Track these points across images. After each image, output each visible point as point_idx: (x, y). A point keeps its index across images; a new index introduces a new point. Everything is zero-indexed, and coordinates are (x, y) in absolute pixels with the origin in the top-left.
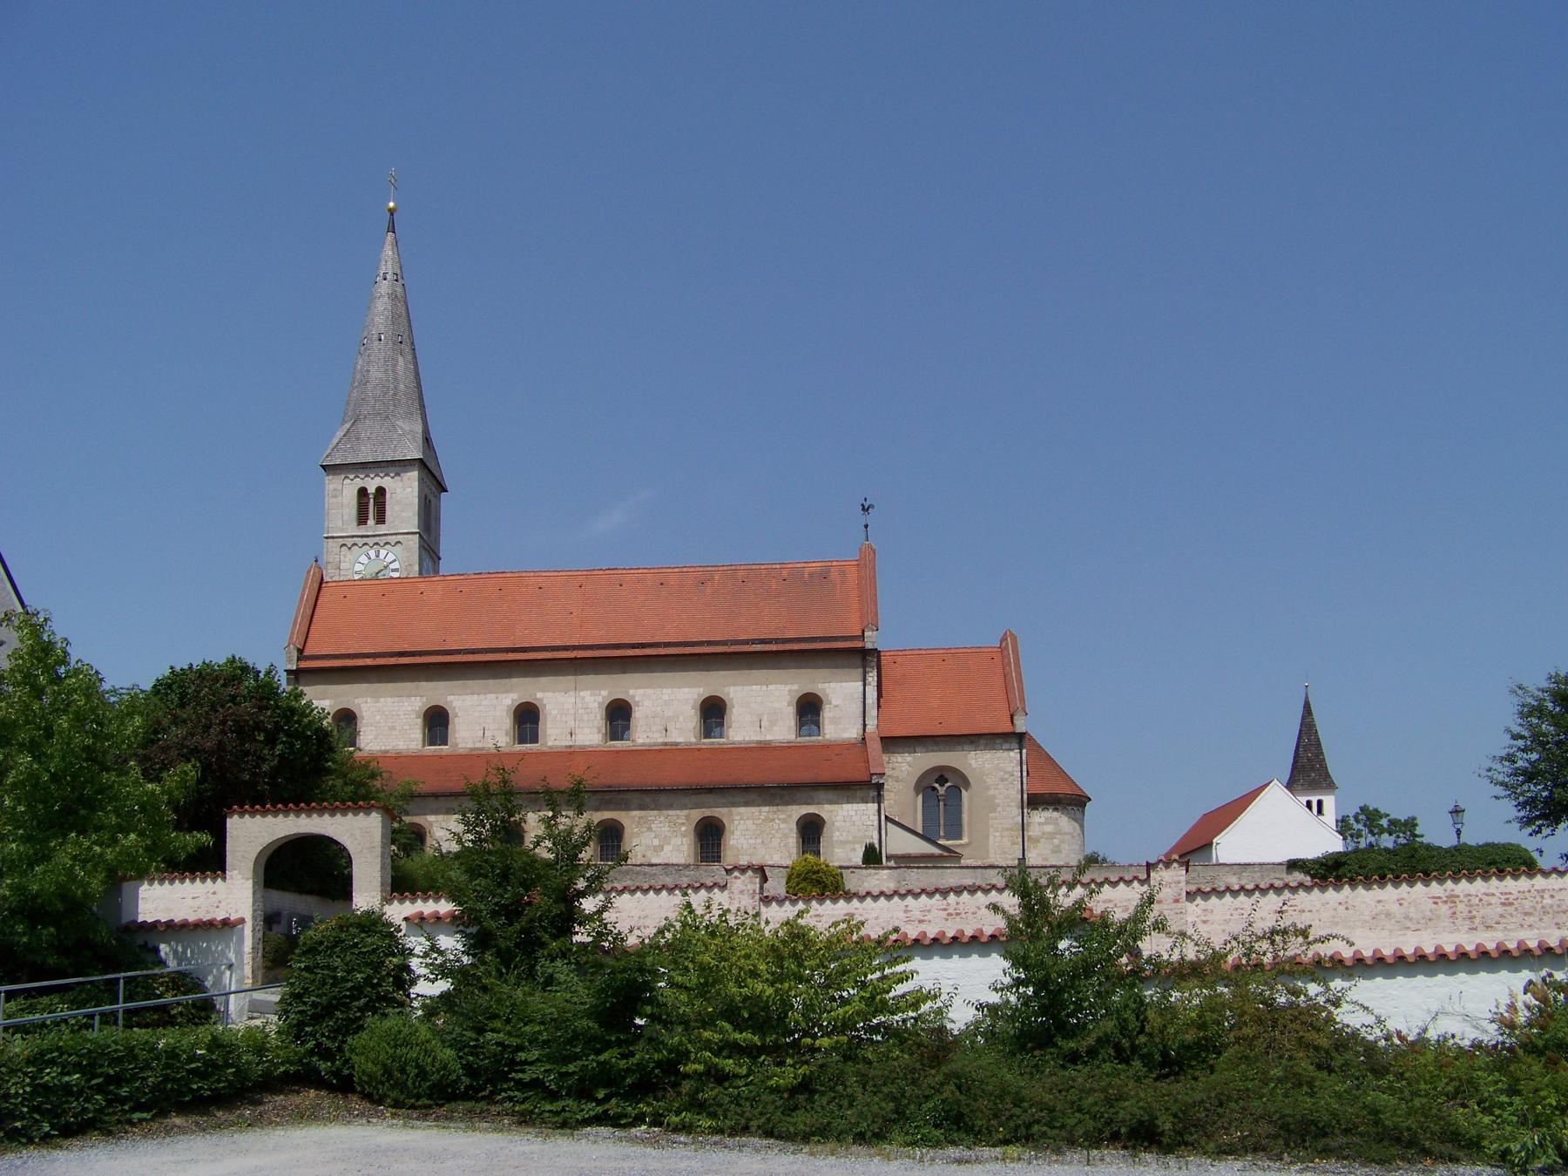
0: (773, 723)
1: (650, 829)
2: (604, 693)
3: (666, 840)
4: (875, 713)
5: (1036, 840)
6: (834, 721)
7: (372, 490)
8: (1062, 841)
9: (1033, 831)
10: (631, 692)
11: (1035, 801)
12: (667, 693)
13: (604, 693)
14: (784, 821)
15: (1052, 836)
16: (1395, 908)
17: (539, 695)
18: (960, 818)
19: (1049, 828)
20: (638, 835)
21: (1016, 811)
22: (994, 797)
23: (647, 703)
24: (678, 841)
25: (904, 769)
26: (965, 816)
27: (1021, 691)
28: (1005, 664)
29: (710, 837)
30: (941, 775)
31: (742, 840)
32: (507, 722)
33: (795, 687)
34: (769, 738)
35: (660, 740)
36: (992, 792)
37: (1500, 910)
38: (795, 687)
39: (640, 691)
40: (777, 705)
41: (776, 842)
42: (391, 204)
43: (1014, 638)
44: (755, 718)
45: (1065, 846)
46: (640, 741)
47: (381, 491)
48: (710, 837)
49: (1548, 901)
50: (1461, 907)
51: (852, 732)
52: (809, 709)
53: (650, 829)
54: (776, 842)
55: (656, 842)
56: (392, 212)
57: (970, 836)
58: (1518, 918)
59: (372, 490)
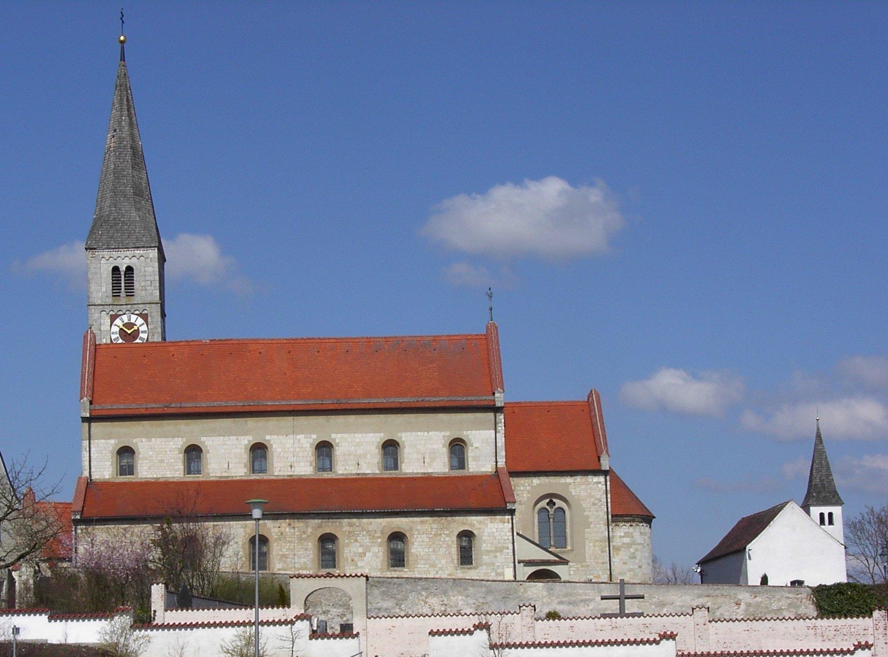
0: (433, 460)
1: (356, 541)
2: (314, 436)
3: (368, 549)
4: (504, 453)
5: (618, 549)
6: (476, 459)
7: (123, 269)
8: (637, 550)
9: (616, 542)
10: (333, 436)
11: (617, 517)
12: (358, 437)
13: (314, 436)
14: (448, 535)
15: (629, 545)
16: (792, 631)
17: (268, 437)
18: (565, 532)
19: (627, 540)
20: (348, 545)
21: (605, 528)
22: (588, 517)
23: (343, 444)
24: (375, 549)
25: (526, 490)
26: (568, 530)
27: (605, 437)
28: (591, 417)
29: (397, 550)
30: (551, 498)
31: (420, 550)
32: (245, 457)
33: (448, 433)
34: (430, 471)
35: (354, 472)
36: (586, 513)
37: (834, 633)
38: (448, 433)
39: (339, 436)
40: (435, 446)
41: (443, 550)
42: (122, 38)
43: (598, 396)
44: (420, 456)
45: (638, 554)
46: (340, 472)
47: (130, 269)
48: (397, 550)
49: (853, 630)
50: (818, 631)
51: (488, 468)
52: (457, 447)
53: (356, 541)
54: (443, 550)
55: (361, 550)
56: (122, 42)
57: (572, 545)
58: (842, 637)
59: (123, 269)
